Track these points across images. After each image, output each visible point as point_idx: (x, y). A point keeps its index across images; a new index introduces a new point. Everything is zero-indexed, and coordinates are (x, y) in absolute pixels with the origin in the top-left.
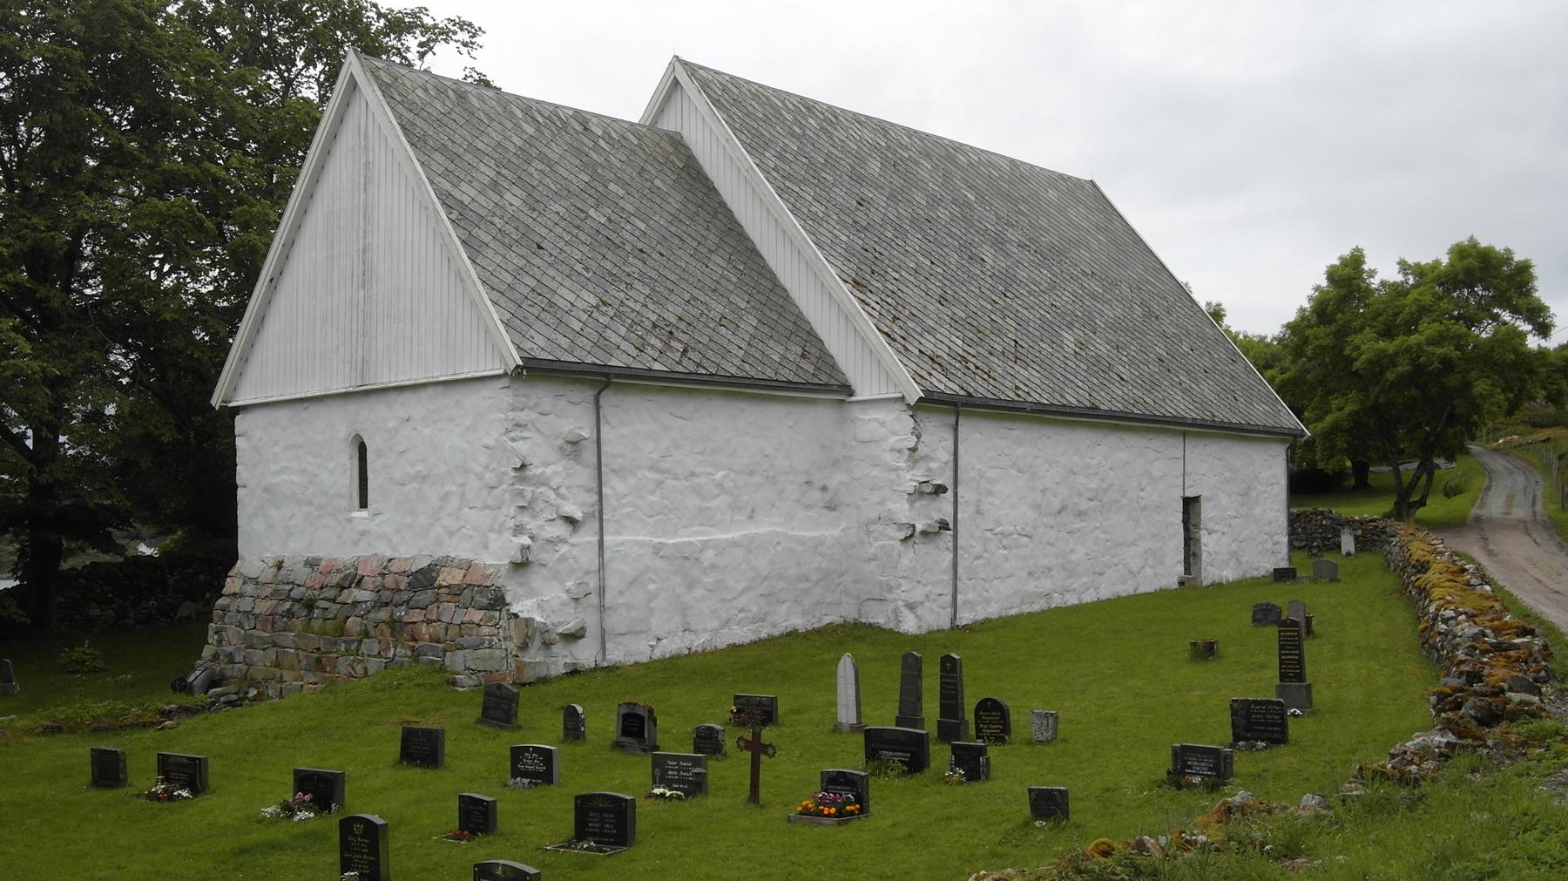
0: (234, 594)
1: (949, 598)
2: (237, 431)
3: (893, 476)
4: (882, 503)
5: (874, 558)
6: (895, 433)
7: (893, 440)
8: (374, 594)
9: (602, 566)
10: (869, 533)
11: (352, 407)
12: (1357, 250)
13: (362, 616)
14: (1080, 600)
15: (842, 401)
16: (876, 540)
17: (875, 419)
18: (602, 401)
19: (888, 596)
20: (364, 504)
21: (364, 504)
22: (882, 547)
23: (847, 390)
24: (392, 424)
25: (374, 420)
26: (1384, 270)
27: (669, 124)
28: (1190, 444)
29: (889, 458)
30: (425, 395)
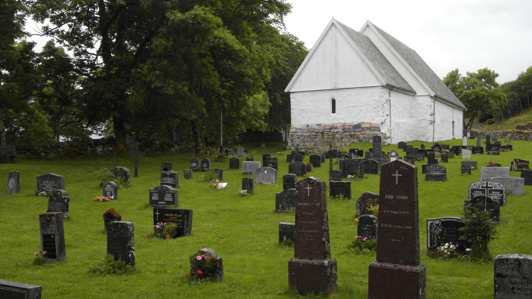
0: (294, 132)
1: (432, 136)
2: (291, 97)
3: (426, 111)
4: (423, 116)
5: (422, 127)
6: (427, 102)
7: (426, 104)
8: (342, 130)
9: (391, 124)
10: (421, 122)
11: (331, 92)
12: (457, 69)
13: (341, 134)
14: (103, 232)
15: (413, 95)
16: (423, 123)
17: (422, 99)
18: (391, 92)
19: (425, 135)
20: (334, 111)
21: (334, 111)
22: (424, 125)
23: (415, 93)
24: (345, 96)
25: (336, 95)
26: (463, 74)
27: (366, 34)
28: (454, 109)
29: (425, 107)
30: (355, 90)
